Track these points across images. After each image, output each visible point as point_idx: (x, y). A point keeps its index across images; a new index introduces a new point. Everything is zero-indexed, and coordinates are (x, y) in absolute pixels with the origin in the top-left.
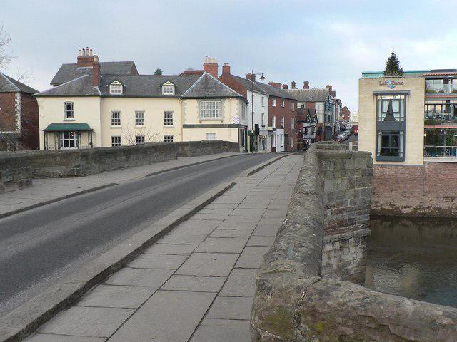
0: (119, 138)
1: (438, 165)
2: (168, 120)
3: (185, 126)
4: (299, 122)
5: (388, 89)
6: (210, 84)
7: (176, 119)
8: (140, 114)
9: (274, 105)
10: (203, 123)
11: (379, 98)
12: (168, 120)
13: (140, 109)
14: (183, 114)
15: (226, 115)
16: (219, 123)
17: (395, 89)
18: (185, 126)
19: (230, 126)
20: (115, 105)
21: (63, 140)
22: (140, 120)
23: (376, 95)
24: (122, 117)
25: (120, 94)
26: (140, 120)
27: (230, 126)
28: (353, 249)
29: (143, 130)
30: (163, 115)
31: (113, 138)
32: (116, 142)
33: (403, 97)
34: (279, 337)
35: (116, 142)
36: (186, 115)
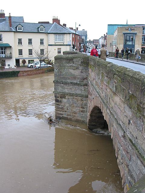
0: (22, 50)
2: (42, 42)
3: (49, 45)
4: (80, 44)
5: (129, 32)
6: (55, 28)
7: (45, 42)
8: (30, 40)
9: (73, 37)
10: (56, 44)
11: (125, 35)
12: (42, 42)
13: (30, 38)
14: (48, 40)
15: (65, 41)
16: (63, 44)
17: (131, 32)
18: (49, 45)
19: (67, 45)
20: (20, 36)
21: (1, 51)
22: (30, 42)
23: (124, 34)
24: (33, 41)
25: (17, 30)
26: (30, 42)
27: (67, 45)
29: (44, 47)
30: (18, 40)
31: (29, 50)
32: (20, 52)
33: (134, 35)
34: (84, 130)
35: (20, 52)
36: (49, 40)
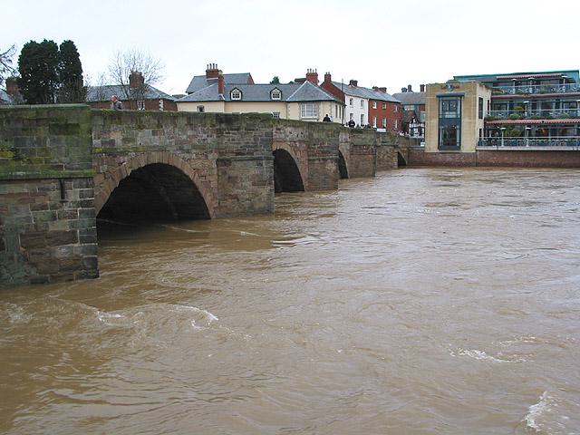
1: (491, 154)
23: (438, 97)
28: (330, 164)
